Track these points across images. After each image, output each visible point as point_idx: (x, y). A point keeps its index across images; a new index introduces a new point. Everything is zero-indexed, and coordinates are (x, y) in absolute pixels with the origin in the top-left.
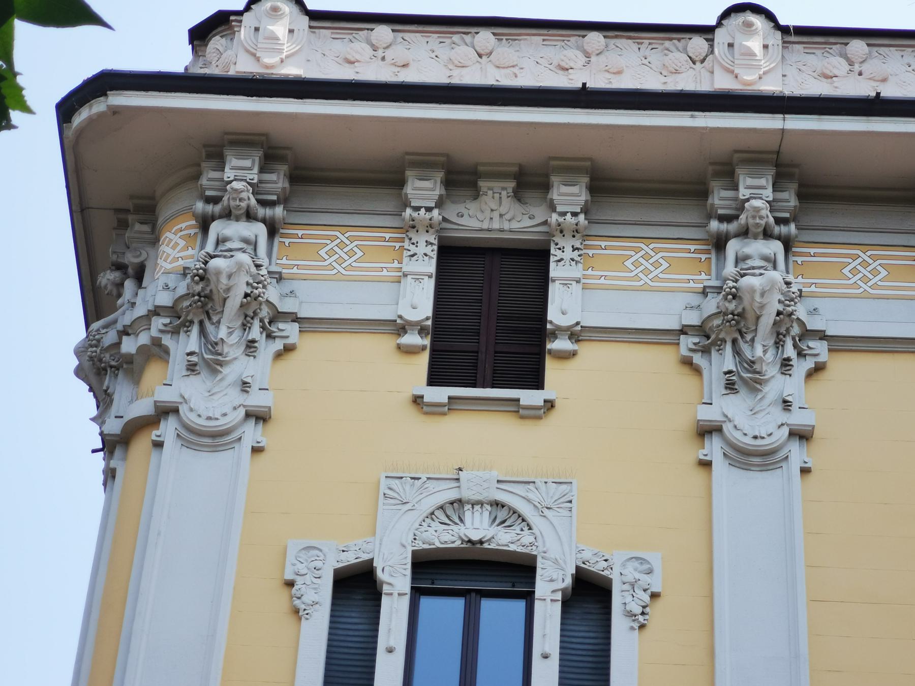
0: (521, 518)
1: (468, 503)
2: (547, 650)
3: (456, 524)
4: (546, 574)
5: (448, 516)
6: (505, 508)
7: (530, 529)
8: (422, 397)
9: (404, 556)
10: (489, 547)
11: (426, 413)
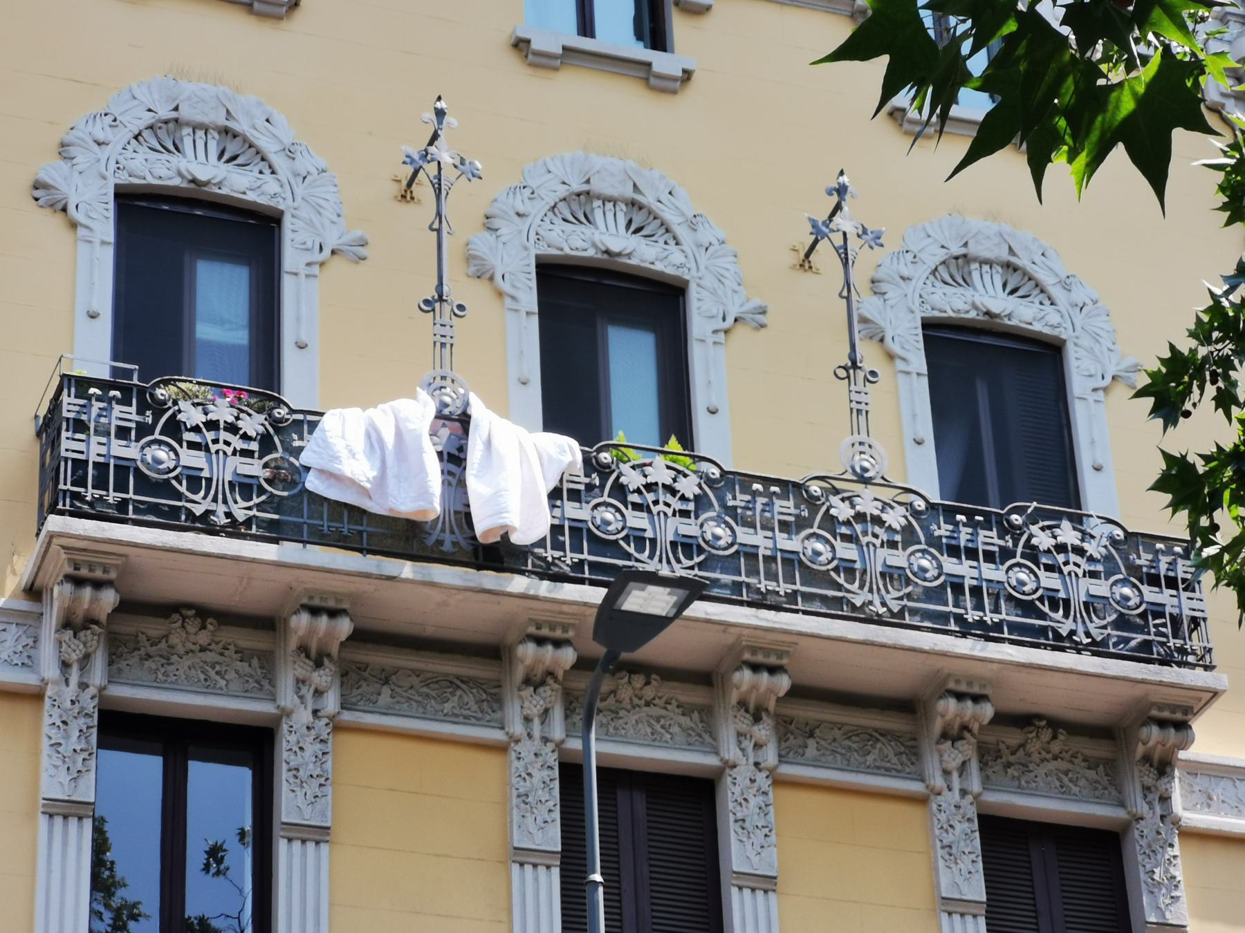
0: (664, 227)
1: (187, 124)
2: (95, 307)
3: (581, 222)
4: (704, 308)
5: (952, 277)
6: (237, 139)
7: (273, 173)
8: (528, 42)
9: (104, 191)
10: (1009, 323)
11: (532, 65)
